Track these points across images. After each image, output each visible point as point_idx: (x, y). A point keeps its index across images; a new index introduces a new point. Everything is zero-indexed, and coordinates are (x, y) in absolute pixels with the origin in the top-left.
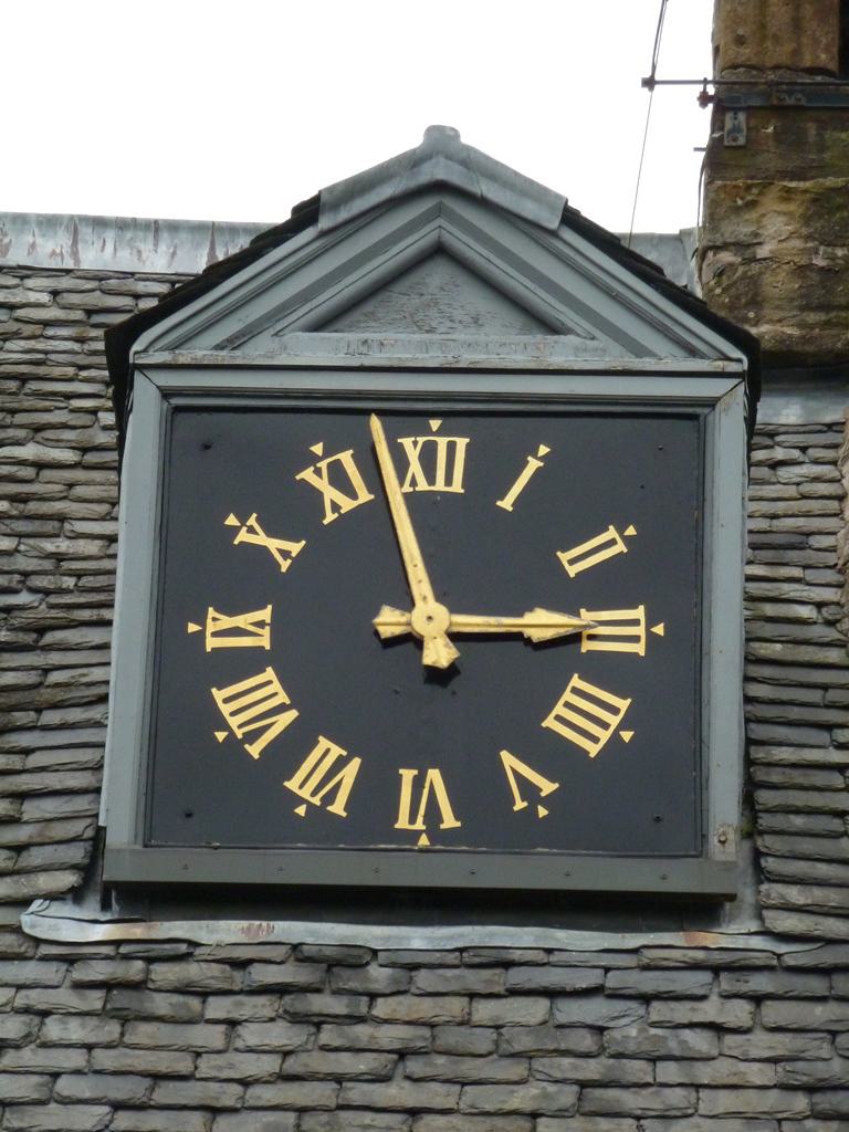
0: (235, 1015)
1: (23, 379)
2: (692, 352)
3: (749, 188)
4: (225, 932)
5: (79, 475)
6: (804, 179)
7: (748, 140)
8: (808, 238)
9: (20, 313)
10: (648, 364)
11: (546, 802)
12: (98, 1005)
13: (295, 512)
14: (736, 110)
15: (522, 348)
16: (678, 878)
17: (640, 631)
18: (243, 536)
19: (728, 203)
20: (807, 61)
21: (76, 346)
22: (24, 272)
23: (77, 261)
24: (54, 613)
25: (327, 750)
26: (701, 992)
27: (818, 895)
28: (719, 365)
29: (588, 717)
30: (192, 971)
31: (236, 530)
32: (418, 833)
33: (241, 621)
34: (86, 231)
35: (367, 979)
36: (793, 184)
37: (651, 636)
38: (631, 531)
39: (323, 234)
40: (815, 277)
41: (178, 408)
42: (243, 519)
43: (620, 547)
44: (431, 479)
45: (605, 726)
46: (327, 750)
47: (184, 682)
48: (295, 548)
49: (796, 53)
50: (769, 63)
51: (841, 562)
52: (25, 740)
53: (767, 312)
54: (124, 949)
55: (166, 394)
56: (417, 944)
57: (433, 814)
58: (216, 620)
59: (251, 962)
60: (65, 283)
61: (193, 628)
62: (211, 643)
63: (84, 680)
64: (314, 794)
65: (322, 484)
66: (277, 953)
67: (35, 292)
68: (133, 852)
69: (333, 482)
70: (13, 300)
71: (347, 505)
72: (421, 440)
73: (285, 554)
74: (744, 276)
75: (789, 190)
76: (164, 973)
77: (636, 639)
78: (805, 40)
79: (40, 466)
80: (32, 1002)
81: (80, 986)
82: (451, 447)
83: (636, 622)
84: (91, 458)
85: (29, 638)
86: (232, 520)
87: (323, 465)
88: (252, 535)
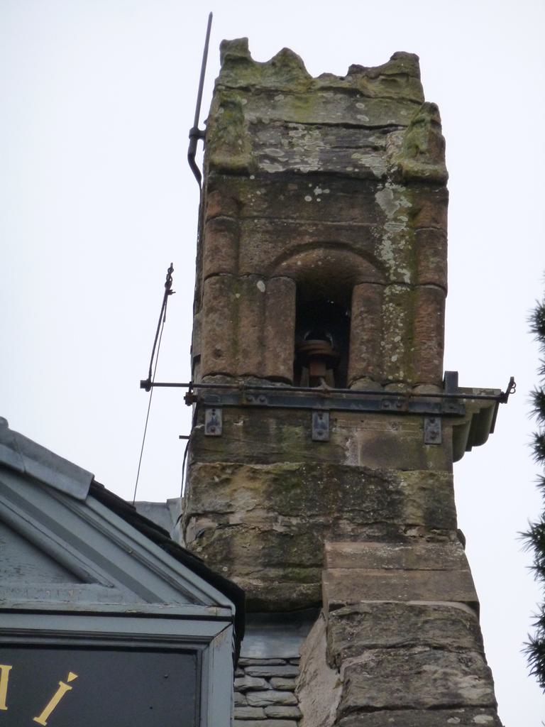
2: (192, 600)
3: (224, 468)
6: (264, 462)
14: (214, 408)
19: (208, 480)
20: (269, 372)
28: (213, 611)
36: (258, 467)
40: (275, 541)
74: (220, 538)
75: (255, 471)
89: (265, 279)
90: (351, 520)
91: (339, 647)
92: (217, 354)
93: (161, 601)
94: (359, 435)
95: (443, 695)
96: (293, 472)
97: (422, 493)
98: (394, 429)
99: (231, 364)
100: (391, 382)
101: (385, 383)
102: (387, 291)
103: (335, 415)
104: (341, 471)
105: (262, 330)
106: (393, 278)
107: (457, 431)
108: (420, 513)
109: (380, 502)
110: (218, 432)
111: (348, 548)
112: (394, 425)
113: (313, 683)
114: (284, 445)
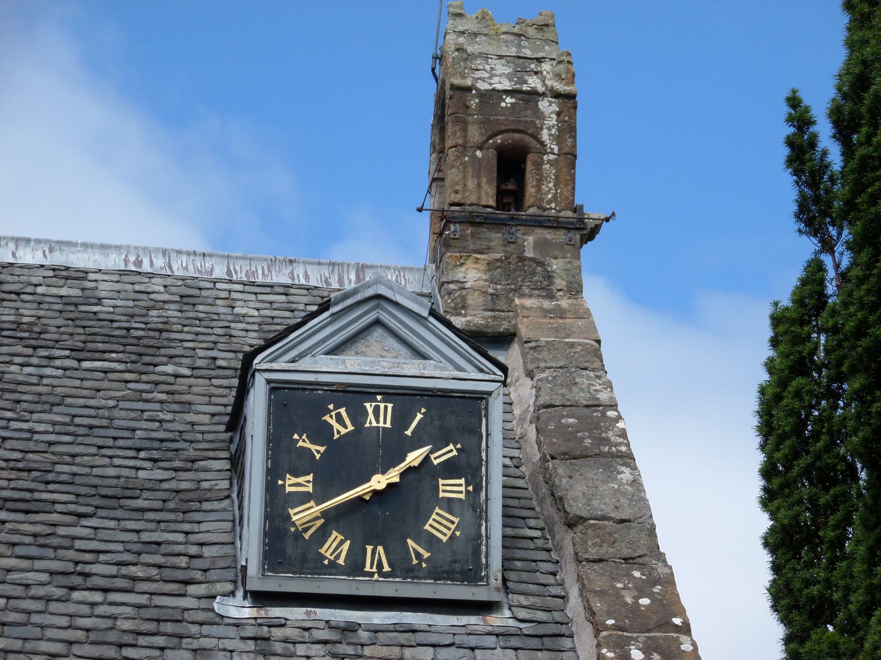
0: (309, 654)
1: (161, 331)
2: (481, 371)
3: (461, 257)
4: (296, 614)
5: (192, 381)
6: (482, 253)
7: (460, 236)
8: (486, 280)
9: (152, 296)
10: (461, 375)
11: (426, 561)
12: (253, 648)
13: (322, 433)
14: (455, 223)
15: (413, 367)
16: (478, 594)
17: (463, 489)
18: (301, 443)
19: (453, 263)
20: (483, 202)
21: (179, 314)
22: (151, 276)
23: (172, 271)
24: (198, 453)
25: (335, 536)
26: (493, 646)
27: (532, 599)
28: (492, 377)
29: (441, 525)
30: (288, 632)
31: (298, 441)
32: (374, 573)
33: (301, 480)
34: (173, 255)
35: (359, 638)
36: (479, 256)
37: (467, 492)
38: (459, 446)
39: (332, 315)
40: (489, 297)
41: (275, 388)
42: (300, 436)
43: (455, 453)
44: (378, 421)
45: (449, 529)
46: (335, 536)
47: (277, 504)
48: (322, 449)
49: (479, 198)
50: (468, 202)
51: (517, 437)
52: (197, 516)
53: (470, 312)
54: (259, 621)
55: (269, 382)
56: (376, 621)
57: (380, 565)
58: (290, 480)
59: (311, 628)
60: (169, 281)
61: (280, 482)
62: (288, 489)
63: (217, 487)
64: (331, 555)
65: (333, 422)
66: (321, 625)
67: (156, 285)
68: (259, 578)
69: (337, 421)
70: (149, 290)
71: (344, 431)
72: (373, 404)
73: (318, 452)
74: (459, 296)
75: (477, 259)
76: (277, 633)
77: (461, 492)
78: (483, 193)
79: (176, 376)
80: (226, 646)
81: (243, 638)
82: (386, 407)
83: (461, 485)
84: (196, 372)
85: (189, 465)
86: (296, 437)
87: (333, 413)
88: (304, 443)
89: (481, 149)
90: (528, 287)
91: (531, 367)
92: (456, 192)
93: (466, 371)
94: (531, 239)
95: (590, 399)
96: (497, 260)
97: (564, 272)
98: (549, 235)
99: (463, 198)
100: (548, 209)
101: (545, 210)
102: (545, 157)
103: (518, 228)
104: (522, 259)
105: (479, 179)
106: (549, 150)
107: (582, 236)
108: (564, 283)
109: (543, 277)
110: (457, 236)
111: (528, 302)
112: (549, 233)
113: (517, 384)
114: (493, 243)
